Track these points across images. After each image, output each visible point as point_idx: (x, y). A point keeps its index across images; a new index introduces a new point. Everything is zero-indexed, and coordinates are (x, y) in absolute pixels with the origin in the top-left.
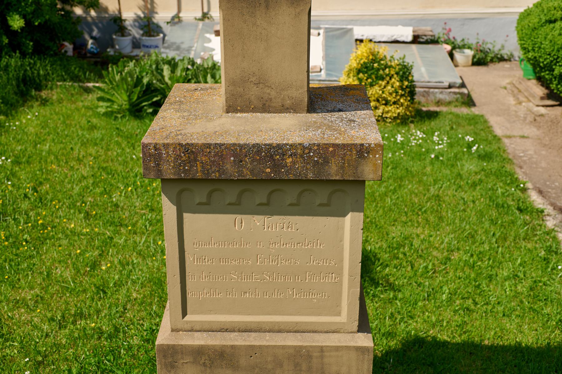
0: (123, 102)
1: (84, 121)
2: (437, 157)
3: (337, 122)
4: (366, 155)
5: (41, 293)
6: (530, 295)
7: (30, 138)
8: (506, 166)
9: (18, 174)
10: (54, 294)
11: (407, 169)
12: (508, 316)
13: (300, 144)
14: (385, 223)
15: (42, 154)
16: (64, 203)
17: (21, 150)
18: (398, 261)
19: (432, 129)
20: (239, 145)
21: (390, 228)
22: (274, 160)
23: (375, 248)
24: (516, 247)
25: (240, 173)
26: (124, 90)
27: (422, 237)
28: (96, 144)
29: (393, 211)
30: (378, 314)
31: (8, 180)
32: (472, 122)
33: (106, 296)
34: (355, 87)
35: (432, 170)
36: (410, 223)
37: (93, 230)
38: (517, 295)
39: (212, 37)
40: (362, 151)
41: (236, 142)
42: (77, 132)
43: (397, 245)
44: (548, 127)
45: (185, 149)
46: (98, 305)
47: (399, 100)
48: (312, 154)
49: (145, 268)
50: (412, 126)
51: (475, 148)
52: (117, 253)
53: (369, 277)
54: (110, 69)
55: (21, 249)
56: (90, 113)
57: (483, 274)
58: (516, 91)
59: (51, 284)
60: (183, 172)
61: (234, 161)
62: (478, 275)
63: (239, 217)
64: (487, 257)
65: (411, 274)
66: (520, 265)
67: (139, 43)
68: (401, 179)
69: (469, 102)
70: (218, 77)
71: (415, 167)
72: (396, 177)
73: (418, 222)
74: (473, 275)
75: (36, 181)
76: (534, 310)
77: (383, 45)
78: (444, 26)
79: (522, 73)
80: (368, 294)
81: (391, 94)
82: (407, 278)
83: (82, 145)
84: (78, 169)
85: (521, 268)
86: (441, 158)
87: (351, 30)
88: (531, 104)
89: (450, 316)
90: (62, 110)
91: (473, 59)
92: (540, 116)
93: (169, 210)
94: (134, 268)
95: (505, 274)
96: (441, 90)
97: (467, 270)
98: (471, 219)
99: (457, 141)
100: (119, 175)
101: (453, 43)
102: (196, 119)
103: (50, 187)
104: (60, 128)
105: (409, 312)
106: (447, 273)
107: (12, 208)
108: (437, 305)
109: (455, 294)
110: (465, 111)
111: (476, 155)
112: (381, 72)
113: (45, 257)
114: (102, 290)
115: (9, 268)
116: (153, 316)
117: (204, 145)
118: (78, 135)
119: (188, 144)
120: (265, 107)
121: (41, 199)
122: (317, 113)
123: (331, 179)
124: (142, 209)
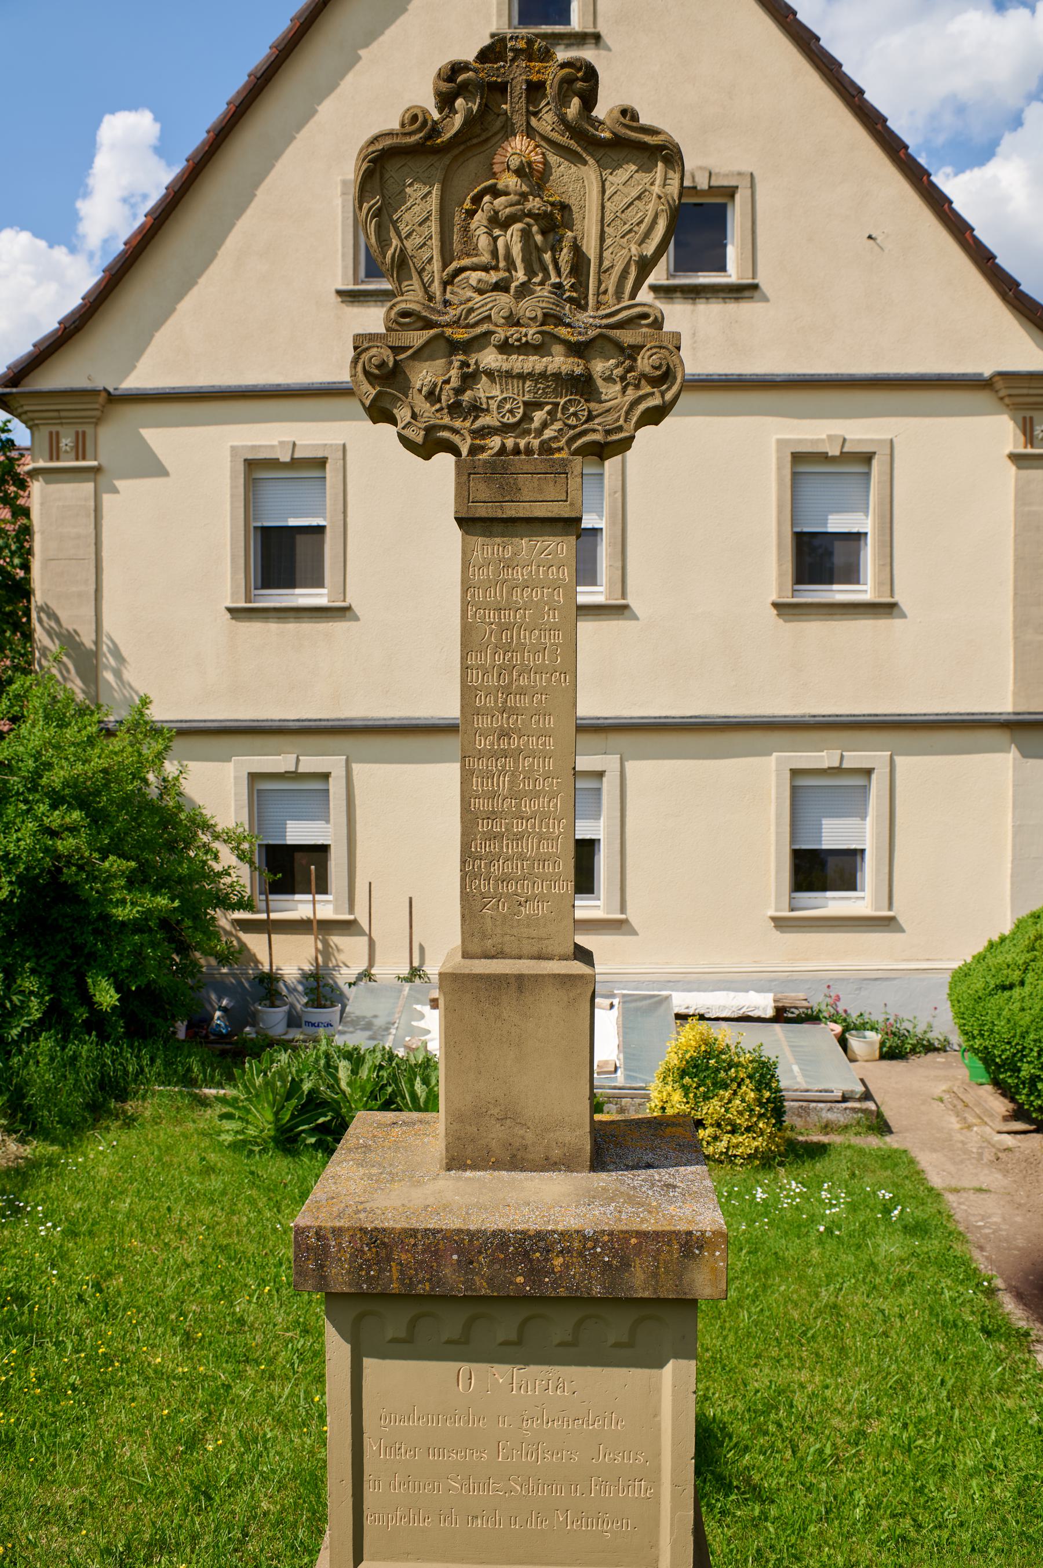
0: (266, 1124)
1: (194, 1158)
2: (829, 1231)
3: (644, 1189)
4: (697, 1252)
5: (92, 1494)
6: (1019, 1506)
7: (99, 1187)
8: (955, 1246)
9: (72, 1255)
10: (116, 1497)
11: (776, 1253)
12: (981, 1552)
13: (578, 1232)
14: (740, 1361)
15: (116, 1218)
16: (147, 1314)
17: (81, 1209)
18: (767, 1438)
19: (818, 1176)
20: (469, 1231)
21: (749, 1371)
22: (531, 1261)
23: (723, 1413)
24: (986, 1407)
25: (469, 1284)
26: (268, 1102)
27: (810, 1388)
28: (212, 1202)
29: (754, 1338)
30: (731, 1551)
31: (53, 1266)
32: (889, 1162)
33: (211, 1505)
34: (674, 1120)
35: (822, 1255)
36: (786, 1362)
37: (195, 1369)
38: (995, 1505)
39: (426, 1009)
40: (690, 1245)
41: (463, 1227)
42: (182, 1178)
43: (764, 1405)
44: (1021, 1171)
45: (371, 1239)
46: (194, 1524)
47: (756, 1123)
48: (599, 1250)
49: (286, 1449)
50: (782, 1171)
51: (896, 1212)
52: (237, 1418)
53: (713, 1473)
54: (247, 1065)
55: (62, 1403)
56: (205, 1143)
57: (929, 1464)
58: (960, 1106)
59: (111, 1477)
60: (365, 1282)
61: (459, 1261)
62: (920, 1465)
63: (465, 1366)
64: (934, 1429)
65: (792, 1466)
66: (996, 1444)
67: (300, 1018)
68: (766, 1273)
69: (881, 1126)
70: (433, 1082)
71: (791, 1250)
72: (757, 1269)
73: (801, 1358)
74: (909, 1468)
75: (101, 1269)
76: (1029, 1538)
77: (724, 1024)
78: (826, 990)
79: (966, 1072)
80: (711, 1507)
81: (741, 1113)
82: (786, 1474)
83: (187, 1203)
84: (177, 1248)
85: (998, 1450)
86: (837, 1233)
87: (668, 998)
88: (988, 1129)
89: (870, 1554)
90: (158, 1136)
91: (881, 1048)
92: (1005, 1150)
93: (337, 1350)
94: (266, 1449)
95: (970, 1463)
96: (829, 1105)
97: (899, 1458)
98: (898, 1352)
99: (865, 1200)
100: (249, 1262)
101: (845, 1020)
102: (393, 1180)
103: (125, 1282)
104: (152, 1169)
105: (792, 1546)
106: (861, 1462)
107: (54, 1321)
108: (845, 1530)
109: (878, 1508)
110: (874, 1142)
111: (899, 1226)
112: (722, 1074)
113: (105, 1423)
114: (204, 1492)
115: (38, 1441)
116: (297, 1551)
117: (405, 1230)
118: (182, 1184)
119: (376, 1229)
120: (516, 1160)
121: (107, 1305)
122: (608, 1171)
123: (635, 1296)
124: (288, 1330)
